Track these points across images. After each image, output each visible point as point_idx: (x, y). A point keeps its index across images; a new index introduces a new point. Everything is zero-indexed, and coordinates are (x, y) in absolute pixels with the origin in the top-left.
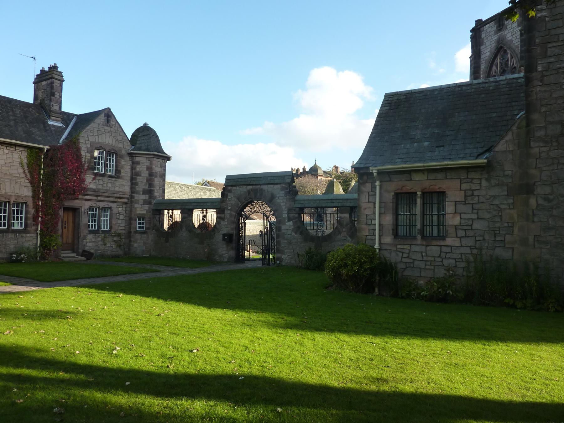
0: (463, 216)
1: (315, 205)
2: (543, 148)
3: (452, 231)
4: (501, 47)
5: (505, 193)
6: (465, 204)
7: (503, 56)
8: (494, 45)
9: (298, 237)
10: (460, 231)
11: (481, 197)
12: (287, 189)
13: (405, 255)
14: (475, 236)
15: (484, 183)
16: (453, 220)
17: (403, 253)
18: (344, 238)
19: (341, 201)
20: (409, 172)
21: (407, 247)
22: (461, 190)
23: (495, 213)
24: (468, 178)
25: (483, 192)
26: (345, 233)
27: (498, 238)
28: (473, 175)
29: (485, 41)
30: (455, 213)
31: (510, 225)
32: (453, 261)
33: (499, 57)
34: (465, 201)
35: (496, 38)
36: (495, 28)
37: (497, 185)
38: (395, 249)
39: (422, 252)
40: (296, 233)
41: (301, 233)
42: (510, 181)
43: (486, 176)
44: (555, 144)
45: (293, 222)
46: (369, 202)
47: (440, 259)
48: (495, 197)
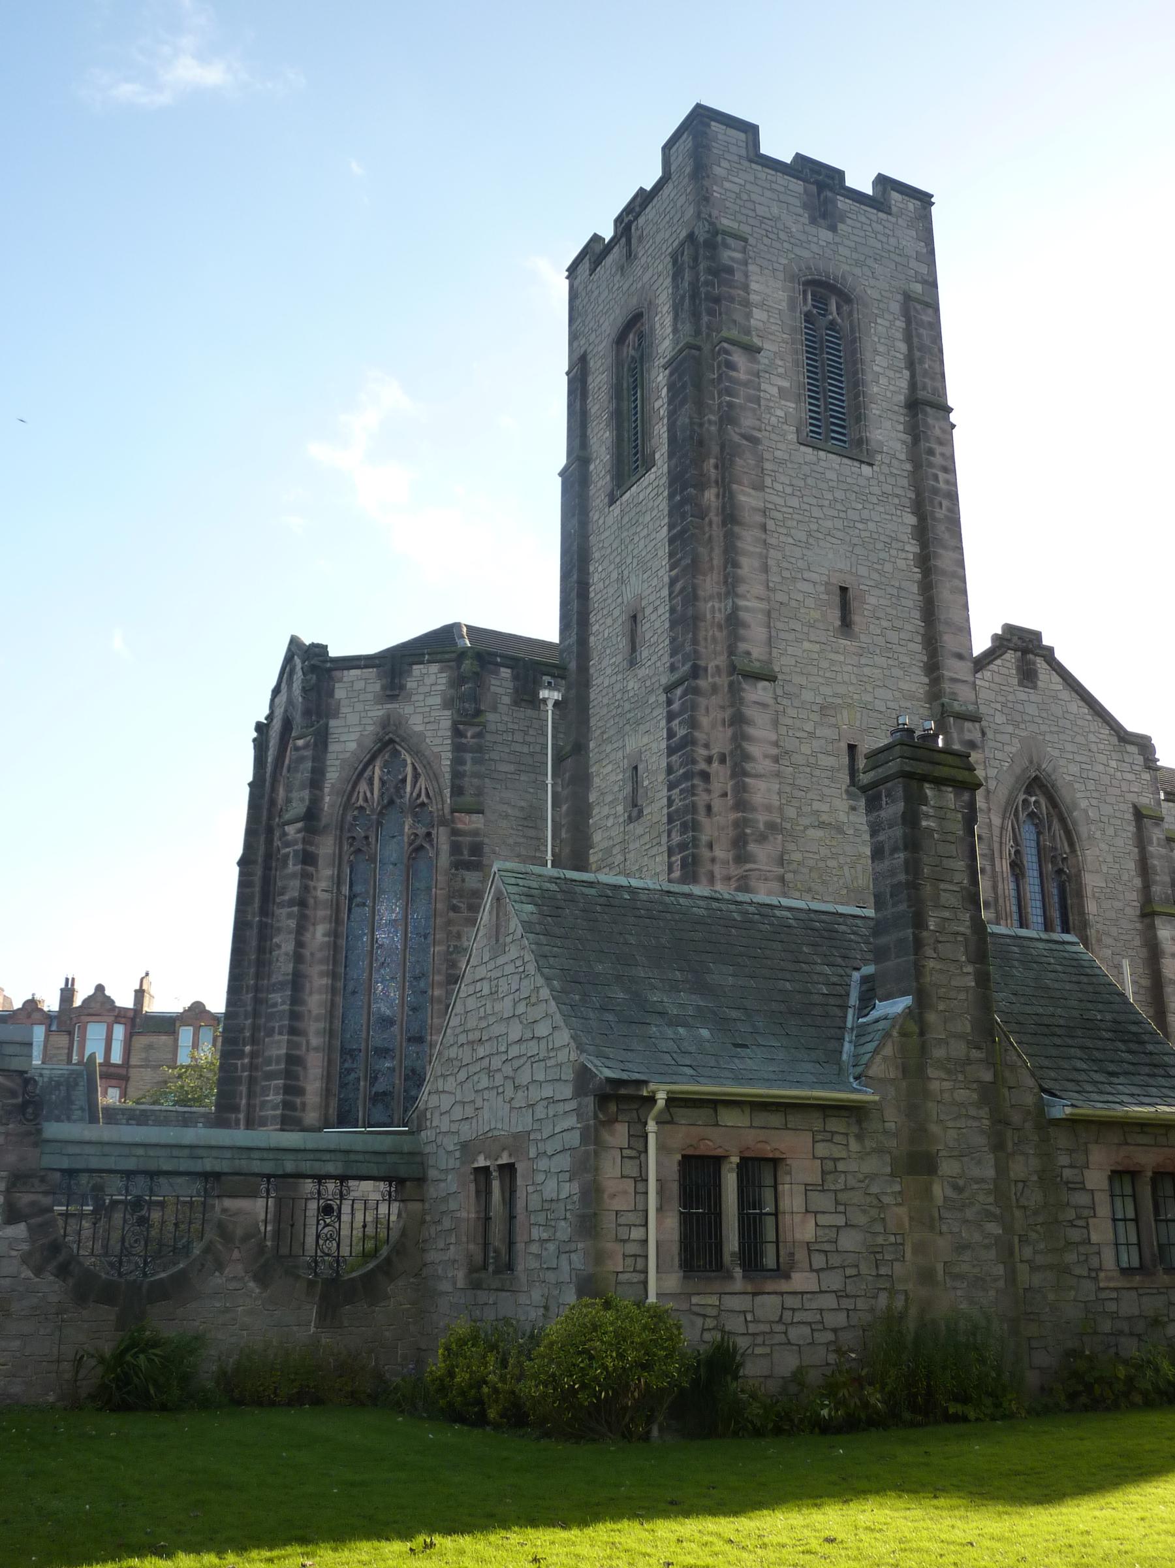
0: (823, 1220)
1: (130, 1164)
2: (944, 1083)
3: (801, 1255)
4: (391, 741)
5: (888, 1170)
6: (823, 1191)
7: (386, 764)
8: (370, 728)
9: (51, 1288)
11: (850, 1177)
12: (13, 1094)
13: (710, 1323)
14: (844, 1267)
15: (854, 1146)
16: (803, 1230)
17: (705, 1316)
19: (228, 1154)
20: (714, 1104)
21: (714, 1300)
22: (814, 1157)
23: (874, 1212)
25: (853, 1167)
26: (240, 1267)
27: (882, 1271)
28: (834, 1125)
29: (343, 710)
30: (807, 1211)
33: (378, 763)
35: (380, 713)
36: (377, 687)
37: (874, 1150)
38: (685, 1307)
39: (744, 1312)
40: (38, 1271)
41: (63, 1271)
42: (893, 1143)
43: (855, 1129)
45: (30, 1229)
46: (622, 1177)
48: (872, 1177)
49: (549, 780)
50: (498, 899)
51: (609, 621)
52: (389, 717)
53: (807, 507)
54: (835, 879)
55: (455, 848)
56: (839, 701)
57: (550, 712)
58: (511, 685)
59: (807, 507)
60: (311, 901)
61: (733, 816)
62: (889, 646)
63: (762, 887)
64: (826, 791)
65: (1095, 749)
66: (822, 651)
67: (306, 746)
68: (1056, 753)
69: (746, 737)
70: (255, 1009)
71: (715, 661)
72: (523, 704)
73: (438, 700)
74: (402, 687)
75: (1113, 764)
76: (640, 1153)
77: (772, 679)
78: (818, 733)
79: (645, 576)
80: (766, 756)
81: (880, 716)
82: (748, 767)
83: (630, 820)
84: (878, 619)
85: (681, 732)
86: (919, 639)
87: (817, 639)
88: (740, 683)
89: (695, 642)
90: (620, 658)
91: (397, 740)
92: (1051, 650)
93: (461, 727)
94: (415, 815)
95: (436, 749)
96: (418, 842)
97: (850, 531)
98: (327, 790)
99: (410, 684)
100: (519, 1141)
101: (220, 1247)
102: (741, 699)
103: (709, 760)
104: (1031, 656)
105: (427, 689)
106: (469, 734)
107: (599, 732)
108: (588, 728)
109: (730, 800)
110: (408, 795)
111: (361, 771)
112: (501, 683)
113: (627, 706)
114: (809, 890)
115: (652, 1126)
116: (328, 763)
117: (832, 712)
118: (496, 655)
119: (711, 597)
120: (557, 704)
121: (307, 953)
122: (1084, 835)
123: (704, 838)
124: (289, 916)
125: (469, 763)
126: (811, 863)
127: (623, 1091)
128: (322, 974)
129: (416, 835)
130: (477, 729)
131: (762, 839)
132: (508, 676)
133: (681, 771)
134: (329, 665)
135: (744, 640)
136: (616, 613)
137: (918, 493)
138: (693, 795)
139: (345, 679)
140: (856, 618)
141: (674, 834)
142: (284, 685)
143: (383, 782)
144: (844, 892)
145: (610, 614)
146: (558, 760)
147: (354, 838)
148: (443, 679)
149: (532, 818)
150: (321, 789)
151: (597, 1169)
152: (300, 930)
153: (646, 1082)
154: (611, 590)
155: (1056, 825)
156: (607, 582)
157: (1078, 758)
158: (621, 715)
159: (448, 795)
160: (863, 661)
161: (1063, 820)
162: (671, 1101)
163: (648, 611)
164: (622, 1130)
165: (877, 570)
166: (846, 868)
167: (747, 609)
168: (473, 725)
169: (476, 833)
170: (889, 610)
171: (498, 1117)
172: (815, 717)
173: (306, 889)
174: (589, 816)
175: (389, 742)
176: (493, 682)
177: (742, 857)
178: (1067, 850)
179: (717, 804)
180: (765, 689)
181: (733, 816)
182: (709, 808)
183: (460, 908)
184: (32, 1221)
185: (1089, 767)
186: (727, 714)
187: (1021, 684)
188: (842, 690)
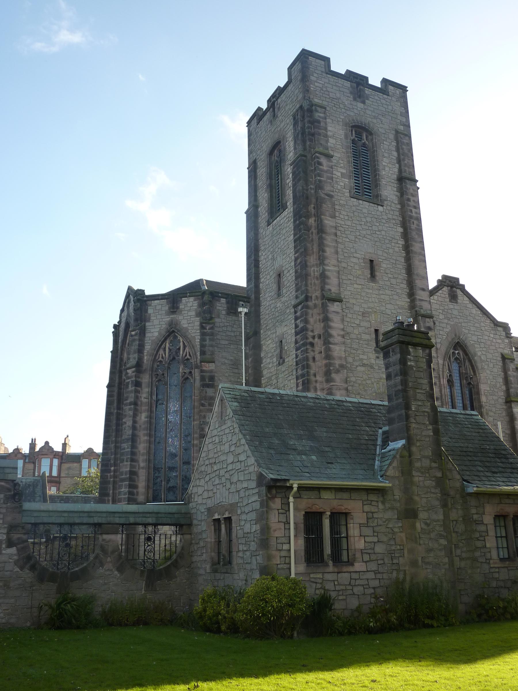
0: (368, 539)
1: (62, 520)
3: (358, 555)
5: (396, 517)
6: (368, 526)
8: (164, 326)
9: (27, 575)
10: (365, 554)
13: (319, 586)
14: (377, 560)
16: (359, 544)
17: (316, 583)
18: (108, 573)
21: (320, 576)
22: (363, 512)
24: (368, 500)
25: (381, 515)
28: (372, 497)
29: (152, 318)
30: (361, 536)
31: (402, 548)
32: (361, 588)
33: (168, 342)
34: (367, 524)
36: (167, 308)
37: (390, 508)
38: (307, 579)
39: (334, 581)
40: (22, 568)
43: (381, 499)
44: (427, 475)
45: (18, 550)
47: (350, 587)
49: (243, 348)
50: (222, 400)
51: (268, 277)
52: (172, 321)
53: (354, 225)
54: (370, 389)
55: (202, 378)
56: (370, 310)
57: (243, 318)
58: (225, 306)
59: (354, 225)
60: (139, 403)
61: (324, 362)
62: (392, 285)
63: (338, 393)
64: (365, 350)
65: (484, 329)
66: (363, 288)
67: (136, 335)
68: (467, 331)
69: (330, 327)
70: (115, 451)
71: (315, 293)
72: (231, 314)
73: (193, 313)
74: (178, 308)
75: (492, 336)
76: (286, 511)
77: (340, 301)
78: (362, 324)
79: (284, 257)
80: (338, 335)
81: (389, 316)
82: (331, 340)
83: (279, 364)
84: (387, 274)
85: (301, 325)
86: (405, 282)
87: (360, 283)
88: (326, 303)
89: (306, 285)
90: (273, 293)
91: (176, 331)
92: (463, 286)
93: (204, 325)
94: (185, 364)
95: (193, 335)
96: (186, 376)
97: (374, 235)
98: (145, 354)
99: (181, 307)
100: (233, 507)
101: (102, 556)
102: (327, 310)
103: (314, 337)
104: (455, 289)
105: (189, 308)
106: (207, 328)
107: (265, 326)
108: (260, 324)
109: (323, 355)
110: (181, 355)
111: (160, 345)
112: (221, 305)
113: (277, 314)
114: (359, 394)
115: (291, 499)
116: (146, 342)
117: (368, 315)
118: (219, 293)
119: (313, 266)
120: (246, 314)
121: (138, 425)
122: (480, 367)
123: (312, 372)
124: (130, 409)
125: (208, 340)
126: (359, 382)
127: (278, 484)
128: (144, 435)
129: (185, 373)
130: (211, 326)
131: (338, 372)
132: (224, 302)
133: (301, 342)
134: (145, 299)
135: (328, 284)
136: (271, 273)
137: (404, 218)
138: (307, 353)
139: (152, 305)
140: (377, 274)
141: (299, 370)
142: (125, 308)
143: (170, 350)
144: (374, 394)
145: (269, 274)
146: (247, 339)
147: (157, 374)
148: (196, 304)
149: (236, 364)
150: (143, 353)
151: (267, 519)
152: (135, 415)
153: (288, 480)
154: (269, 263)
155: (467, 363)
156: (267, 260)
157: (476, 333)
158: (274, 318)
159: (199, 355)
160: (381, 292)
161: (470, 361)
162: (300, 488)
163: (285, 272)
164: (278, 501)
165: (386, 252)
166: (375, 384)
167: (329, 270)
168: (209, 324)
169: (211, 371)
170: (392, 270)
171: (223, 496)
172: (360, 317)
173: (137, 397)
174: (261, 363)
175: (172, 332)
176: (218, 304)
177: (329, 380)
178: (472, 374)
179: (317, 357)
180: (337, 306)
181: (324, 362)
182: (314, 358)
183: (205, 404)
184: (18, 546)
185: (481, 337)
186: (321, 317)
187: (450, 301)
188: (372, 305)
